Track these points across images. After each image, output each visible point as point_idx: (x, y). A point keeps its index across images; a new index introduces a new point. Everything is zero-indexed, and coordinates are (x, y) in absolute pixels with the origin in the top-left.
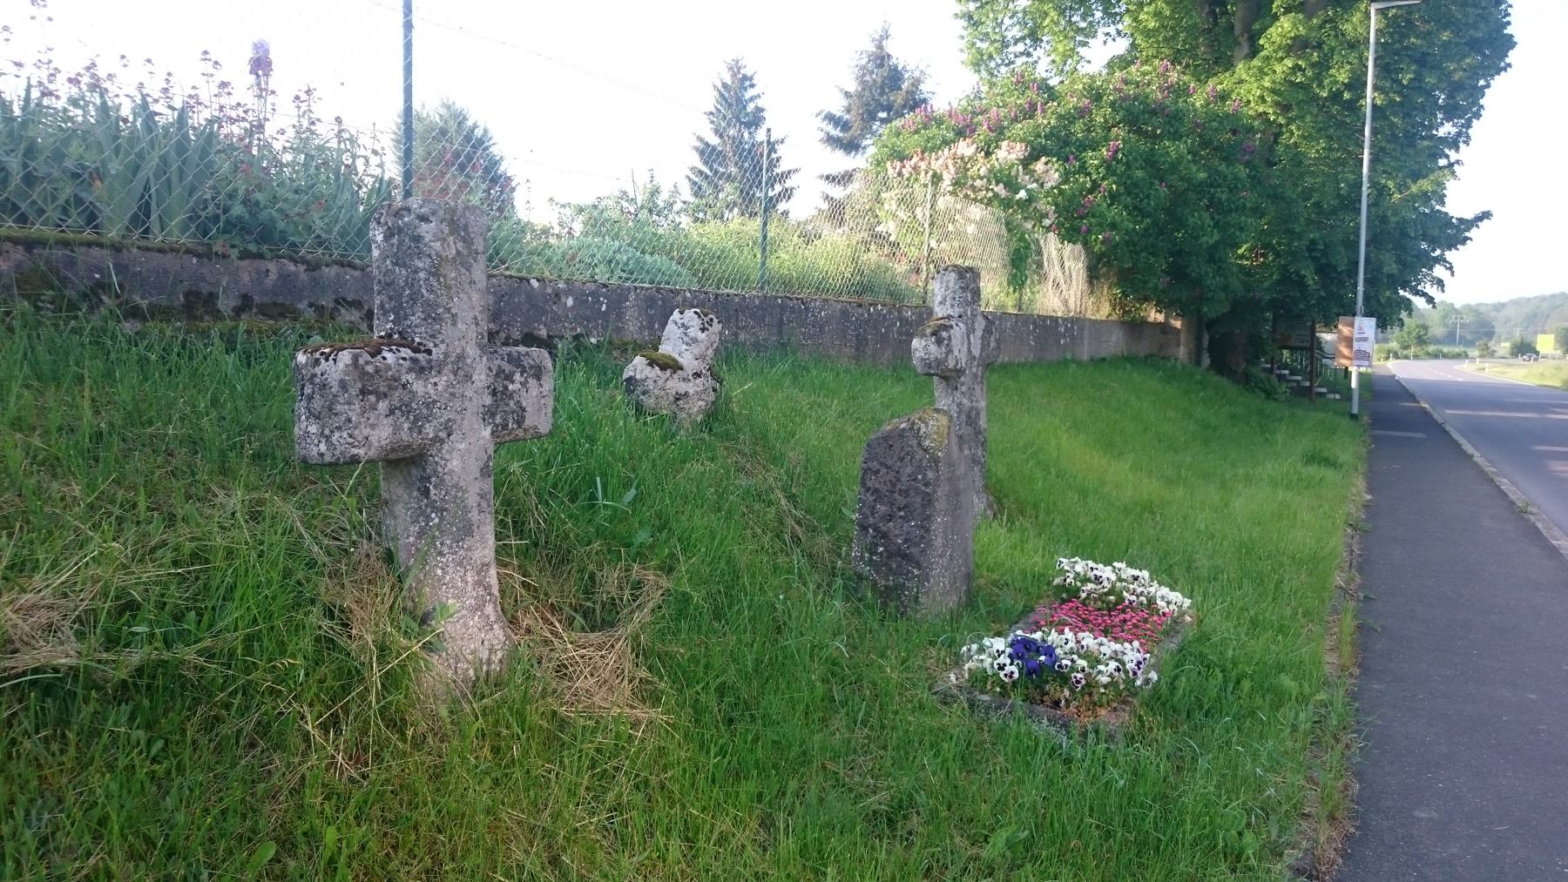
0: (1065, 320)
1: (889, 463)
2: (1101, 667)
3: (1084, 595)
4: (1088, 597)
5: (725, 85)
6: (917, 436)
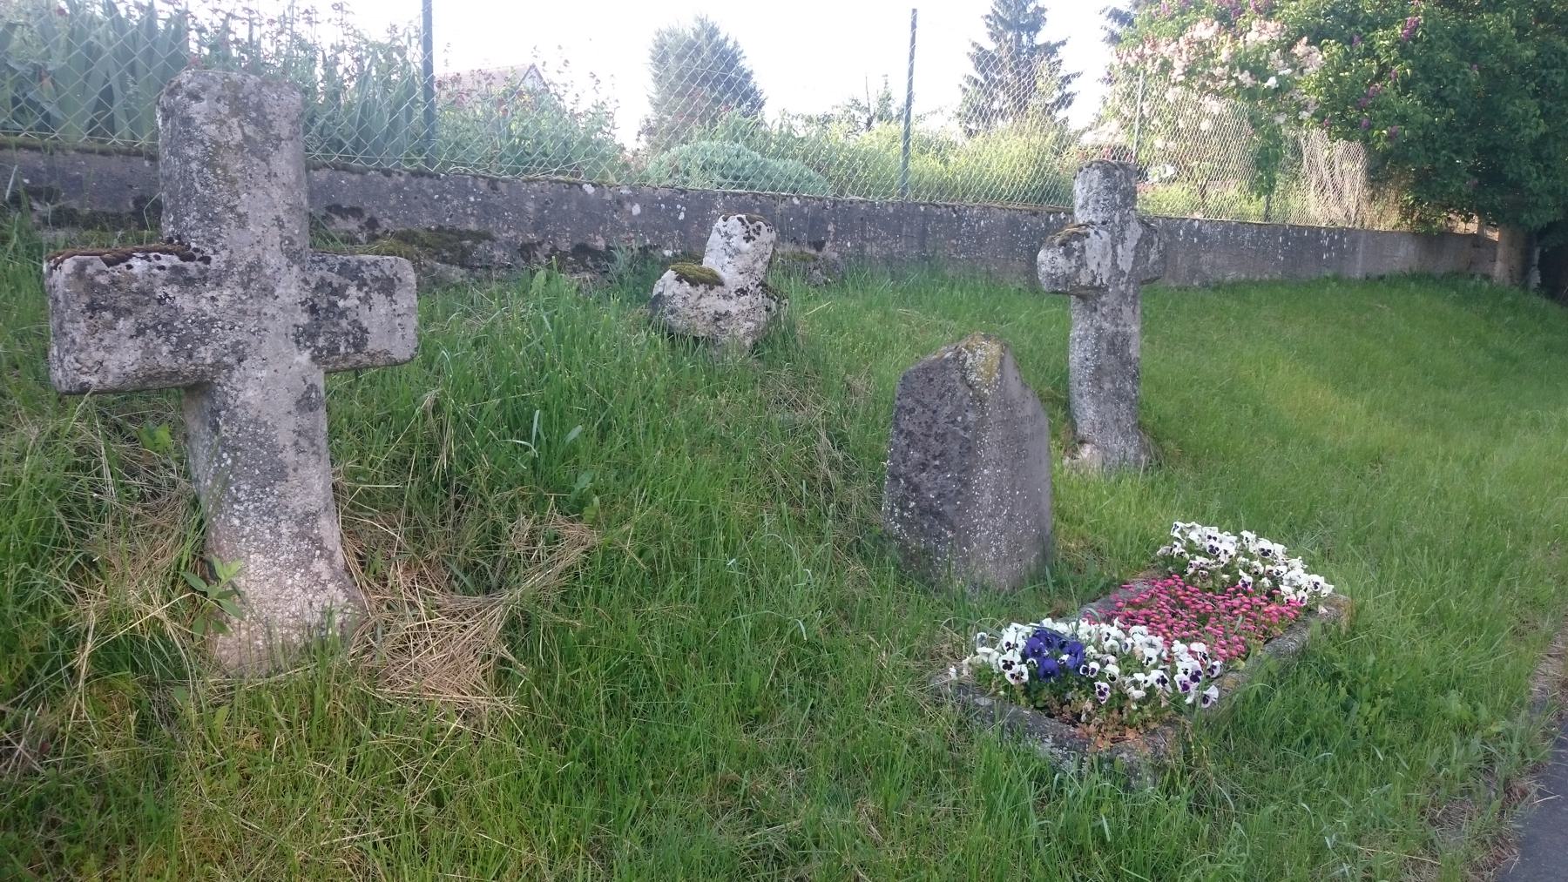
0: (1329, 230)
1: (926, 401)
2: (1140, 677)
3: (1191, 571)
4: (1195, 575)
6: (962, 369)
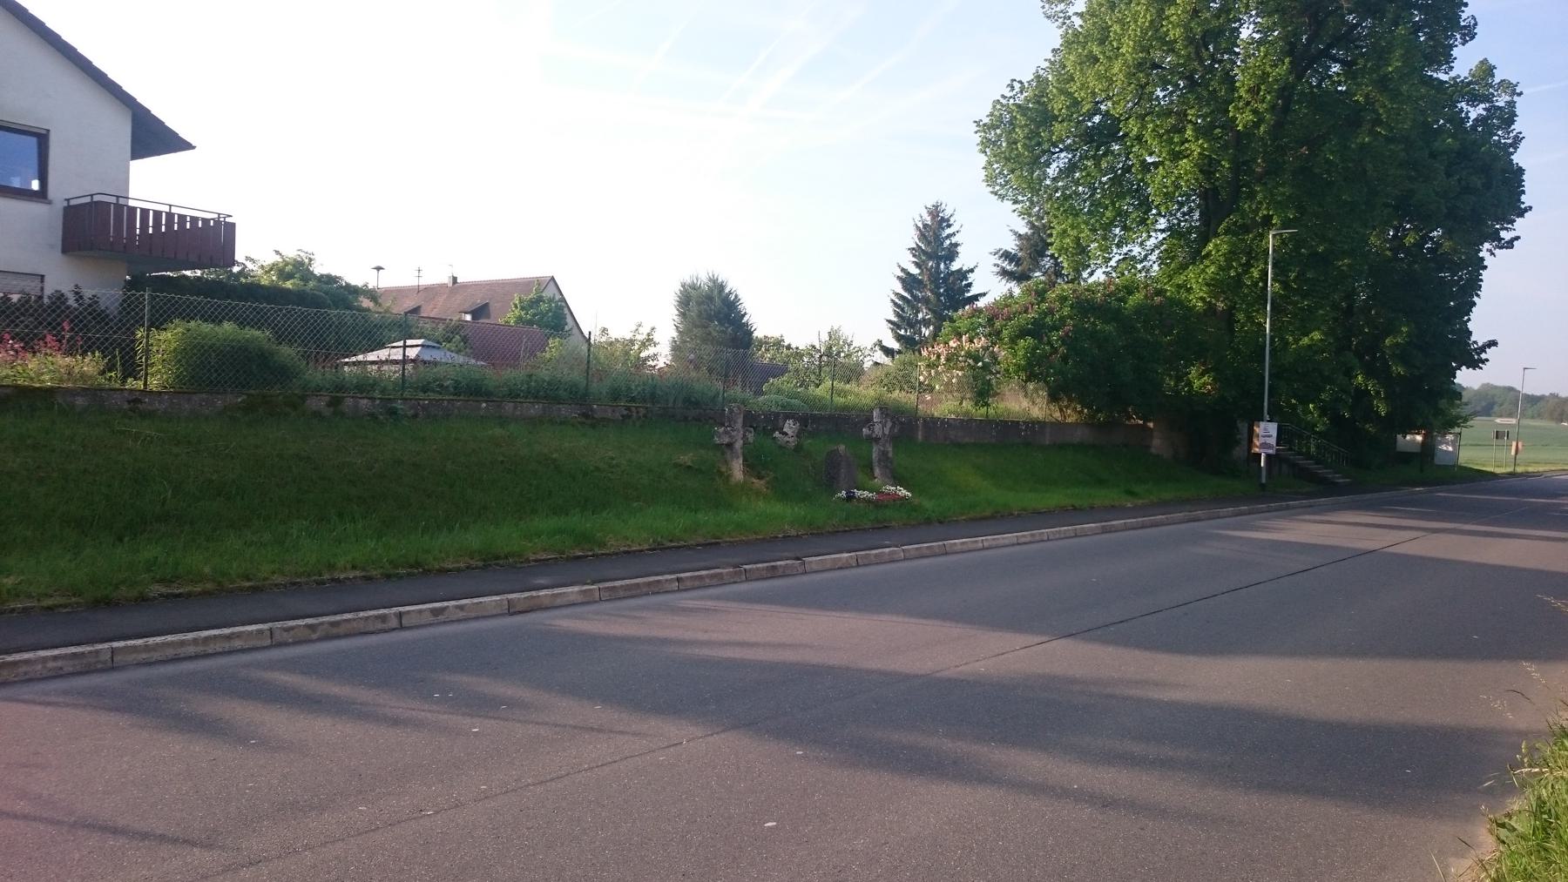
5: (925, 226)
